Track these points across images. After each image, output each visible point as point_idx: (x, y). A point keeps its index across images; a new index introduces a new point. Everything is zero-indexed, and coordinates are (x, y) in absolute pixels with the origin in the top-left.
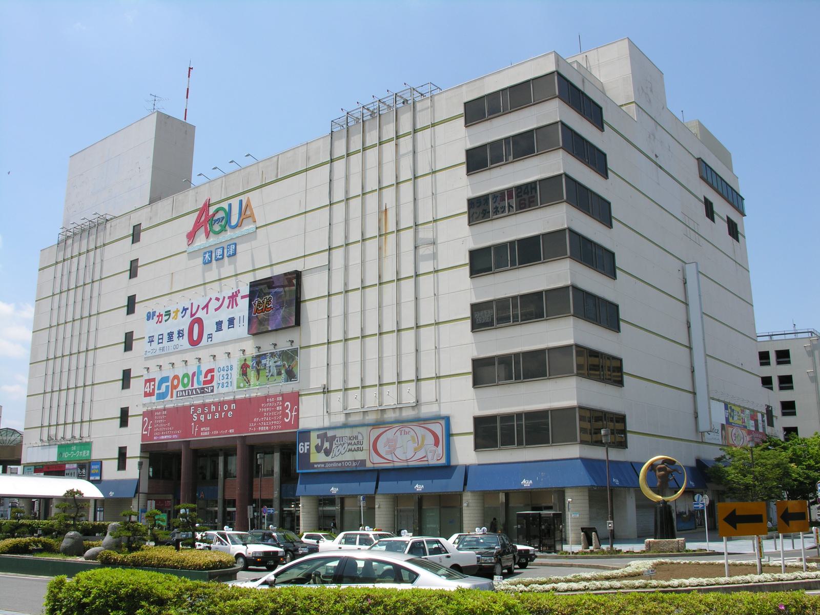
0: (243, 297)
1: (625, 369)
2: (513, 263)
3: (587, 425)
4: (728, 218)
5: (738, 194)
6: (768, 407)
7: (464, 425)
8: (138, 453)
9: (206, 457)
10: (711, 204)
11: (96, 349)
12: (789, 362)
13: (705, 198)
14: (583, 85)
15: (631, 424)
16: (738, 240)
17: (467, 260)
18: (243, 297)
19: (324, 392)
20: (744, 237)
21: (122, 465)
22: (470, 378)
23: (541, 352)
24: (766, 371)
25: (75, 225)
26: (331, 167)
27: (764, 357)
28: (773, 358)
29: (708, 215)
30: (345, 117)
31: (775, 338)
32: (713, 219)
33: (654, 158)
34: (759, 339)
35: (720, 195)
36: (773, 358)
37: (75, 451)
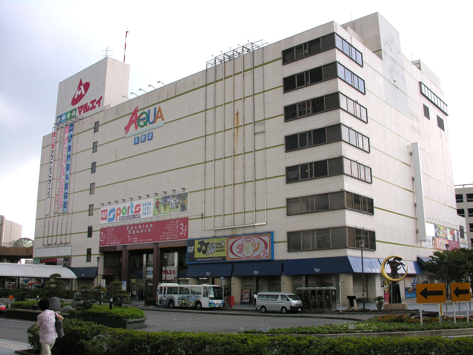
1: (375, 205)
7: (281, 236)
8: (98, 252)
24: (462, 206)
27: (459, 198)
28: (465, 198)
35: (433, 109)
36: (465, 198)
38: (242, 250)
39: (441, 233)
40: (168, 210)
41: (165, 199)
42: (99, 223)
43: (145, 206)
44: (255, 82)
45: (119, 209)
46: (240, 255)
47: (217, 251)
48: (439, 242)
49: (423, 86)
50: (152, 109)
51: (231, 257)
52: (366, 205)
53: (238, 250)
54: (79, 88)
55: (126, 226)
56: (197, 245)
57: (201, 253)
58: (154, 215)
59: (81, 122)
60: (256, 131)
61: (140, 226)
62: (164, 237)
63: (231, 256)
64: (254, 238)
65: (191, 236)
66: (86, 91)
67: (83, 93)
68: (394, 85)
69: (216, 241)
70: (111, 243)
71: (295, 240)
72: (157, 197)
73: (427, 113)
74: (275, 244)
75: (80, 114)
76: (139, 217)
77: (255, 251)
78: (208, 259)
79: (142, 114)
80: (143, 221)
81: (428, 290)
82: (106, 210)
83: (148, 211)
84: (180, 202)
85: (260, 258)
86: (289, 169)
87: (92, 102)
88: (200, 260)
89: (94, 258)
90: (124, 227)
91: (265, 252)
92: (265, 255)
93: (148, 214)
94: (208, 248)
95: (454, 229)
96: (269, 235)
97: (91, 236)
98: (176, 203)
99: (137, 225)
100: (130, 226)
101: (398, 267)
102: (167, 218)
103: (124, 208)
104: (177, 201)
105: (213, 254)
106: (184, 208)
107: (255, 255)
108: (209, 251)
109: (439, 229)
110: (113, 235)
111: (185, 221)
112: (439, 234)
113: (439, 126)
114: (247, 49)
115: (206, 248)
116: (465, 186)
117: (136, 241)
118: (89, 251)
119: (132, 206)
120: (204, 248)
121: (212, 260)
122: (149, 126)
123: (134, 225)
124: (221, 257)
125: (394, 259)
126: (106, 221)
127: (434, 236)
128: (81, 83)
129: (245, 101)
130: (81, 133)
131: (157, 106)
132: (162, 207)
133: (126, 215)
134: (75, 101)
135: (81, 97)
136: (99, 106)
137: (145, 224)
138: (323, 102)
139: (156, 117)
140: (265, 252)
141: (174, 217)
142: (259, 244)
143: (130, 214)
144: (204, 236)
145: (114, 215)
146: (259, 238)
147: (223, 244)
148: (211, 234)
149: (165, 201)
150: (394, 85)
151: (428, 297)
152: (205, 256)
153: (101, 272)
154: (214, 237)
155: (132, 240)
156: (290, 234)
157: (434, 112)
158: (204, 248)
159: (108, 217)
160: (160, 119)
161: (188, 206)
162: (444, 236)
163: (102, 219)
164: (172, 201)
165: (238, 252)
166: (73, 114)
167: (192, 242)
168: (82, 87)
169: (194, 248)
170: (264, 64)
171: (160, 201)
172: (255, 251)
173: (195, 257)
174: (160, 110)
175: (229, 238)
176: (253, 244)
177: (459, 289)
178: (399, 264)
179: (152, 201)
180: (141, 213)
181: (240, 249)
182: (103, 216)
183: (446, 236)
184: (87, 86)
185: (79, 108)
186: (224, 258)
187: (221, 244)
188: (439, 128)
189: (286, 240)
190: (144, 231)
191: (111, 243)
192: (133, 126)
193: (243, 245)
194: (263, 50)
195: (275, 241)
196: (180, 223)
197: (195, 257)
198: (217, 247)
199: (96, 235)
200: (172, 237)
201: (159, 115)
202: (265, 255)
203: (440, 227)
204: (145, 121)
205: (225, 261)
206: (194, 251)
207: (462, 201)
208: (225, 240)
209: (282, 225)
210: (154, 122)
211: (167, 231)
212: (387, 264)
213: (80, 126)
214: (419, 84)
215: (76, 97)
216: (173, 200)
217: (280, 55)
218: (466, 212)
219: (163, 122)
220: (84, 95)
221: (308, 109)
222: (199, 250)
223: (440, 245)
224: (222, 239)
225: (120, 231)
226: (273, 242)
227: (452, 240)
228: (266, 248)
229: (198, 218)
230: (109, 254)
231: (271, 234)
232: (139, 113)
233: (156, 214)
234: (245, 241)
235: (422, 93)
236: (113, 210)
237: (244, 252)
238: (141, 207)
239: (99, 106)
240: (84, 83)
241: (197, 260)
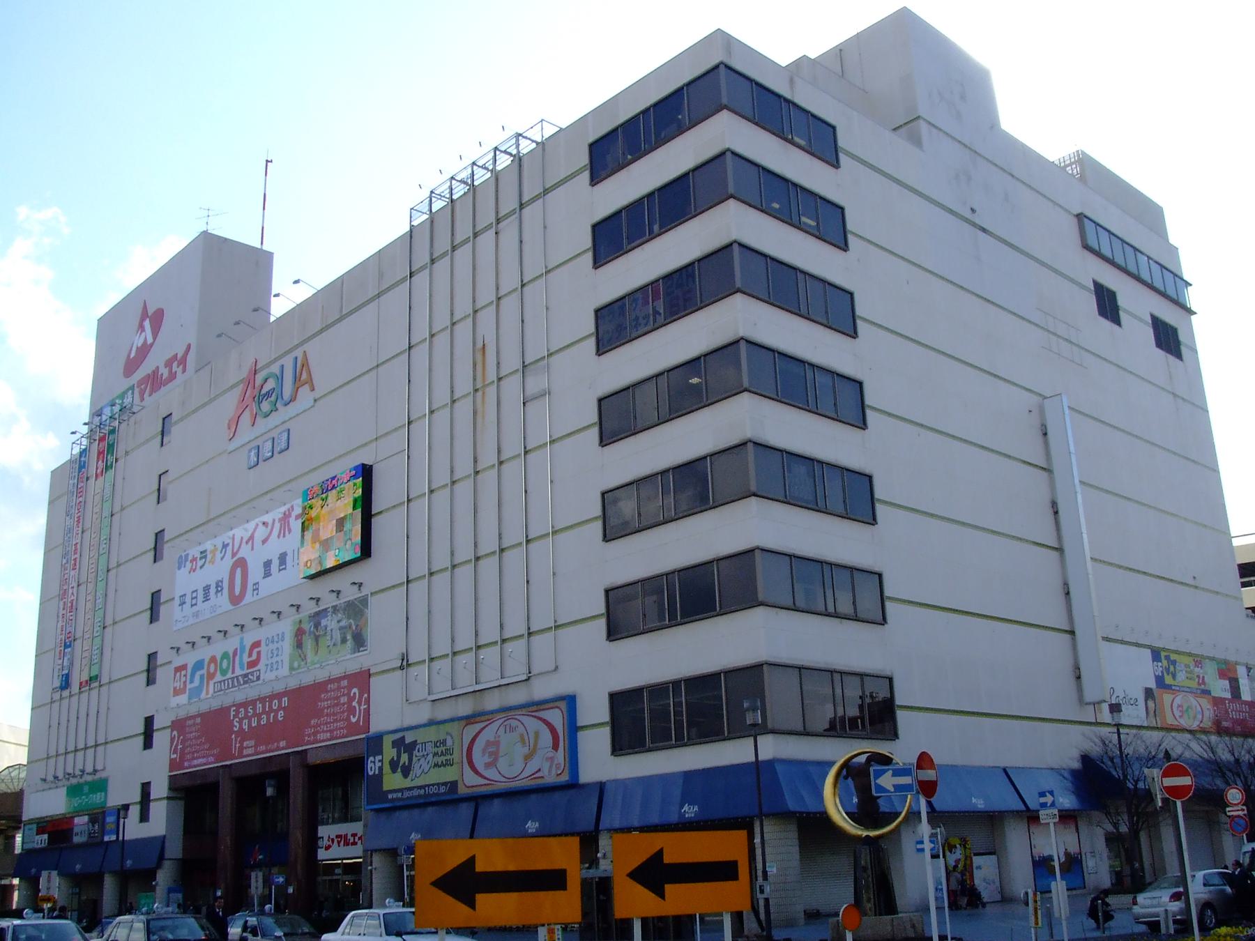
19: (401, 668)
32: (1116, 320)
33: (968, 214)
38: (496, 759)
39: (1181, 676)
40: (323, 650)
41: (317, 617)
42: (170, 703)
43: (271, 646)
44: (526, 247)
45: (213, 659)
46: (491, 773)
47: (436, 765)
48: (1175, 705)
49: (1089, 227)
50: (288, 362)
51: (470, 782)
53: (487, 759)
54: (141, 328)
55: (228, 709)
56: (389, 752)
57: (399, 775)
58: (292, 669)
60: (529, 392)
61: (259, 705)
62: (315, 734)
63: (470, 779)
64: (526, 720)
65: (376, 726)
66: (155, 334)
67: (150, 340)
68: (974, 225)
69: (432, 734)
70: (195, 762)
71: (639, 718)
72: (297, 617)
73: (1107, 305)
74: (580, 734)
75: (142, 400)
76: (258, 678)
77: (528, 758)
78: (416, 793)
79: (266, 380)
80: (266, 691)
81: (667, 859)
82: (184, 667)
83: (279, 659)
84: (350, 626)
85: (540, 781)
87: (169, 364)
88: (395, 796)
89: (159, 810)
90: (223, 712)
91: (552, 759)
92: (554, 772)
93: (280, 671)
94: (415, 759)
95: (1237, 663)
96: (563, 705)
98: (341, 628)
99: (253, 703)
100: (239, 706)
102: (321, 675)
103: (225, 655)
104: (343, 623)
105: (427, 775)
106: (359, 641)
107: (527, 773)
108: (416, 770)
109: (1174, 663)
110: (199, 737)
111: (362, 679)
112: (1174, 676)
113: (1159, 344)
115: (410, 760)
117: (250, 751)
118: (146, 787)
119: (243, 647)
120: (404, 758)
121: (425, 796)
122: (284, 413)
123: (244, 705)
124: (445, 784)
125: (869, 760)
126: (183, 699)
127: (1152, 684)
128: (145, 314)
129: (502, 307)
131: (299, 353)
132: (308, 643)
133: (229, 675)
134: (131, 366)
135: (144, 350)
136: (184, 371)
137: (272, 697)
138: (694, 282)
139: (297, 382)
140: (552, 759)
141: (337, 671)
142: (537, 734)
143: (239, 672)
144: (408, 722)
145: (202, 676)
146: (540, 719)
147: (449, 742)
148: (422, 714)
149: (317, 625)
150: (974, 225)
151: (669, 888)
152: (407, 783)
153: (175, 850)
154: (431, 723)
155: (242, 748)
156: (618, 700)
157: (1129, 295)
158: (404, 758)
159: (189, 686)
160: (307, 387)
161: (371, 634)
162: (1193, 684)
163: (177, 692)
164: (330, 623)
165: (488, 765)
166: (127, 401)
167: (375, 744)
168: (147, 324)
169: (381, 761)
170: (546, 191)
171: (307, 626)
172: (528, 758)
173: (385, 788)
174: (305, 364)
175: (463, 723)
176: (522, 736)
179: (286, 627)
180: (261, 666)
181: (491, 754)
182: (177, 685)
183: (1204, 683)
184: (157, 319)
185: (140, 383)
186: (453, 785)
187: (444, 742)
188: (1160, 353)
189: (607, 718)
190: (268, 719)
191: (195, 762)
192: (246, 418)
193: (497, 743)
194: (544, 150)
195: (579, 724)
196: (350, 688)
197: (385, 788)
198: (435, 754)
199: (162, 739)
200: (331, 731)
201: (304, 376)
202: (554, 772)
203: (1173, 657)
204: (273, 398)
205: (456, 796)
206: (381, 769)
208: (454, 728)
209: (603, 669)
210: (293, 399)
211: (318, 713)
212: (846, 778)
214: (1075, 220)
215: (133, 355)
216: (336, 618)
217: (584, 159)
219: (312, 396)
220: (152, 345)
221: (654, 308)
222: (394, 765)
223: (1177, 714)
224: (447, 727)
225: (214, 724)
226: (574, 729)
227: (1228, 696)
228: (555, 747)
229: (394, 669)
230: (193, 794)
231: (570, 701)
232: (259, 378)
233: (296, 665)
234: (502, 729)
235: (1086, 247)
236: (199, 665)
237: (502, 764)
238: (263, 648)
239: (184, 371)
240: (150, 312)
241: (390, 796)
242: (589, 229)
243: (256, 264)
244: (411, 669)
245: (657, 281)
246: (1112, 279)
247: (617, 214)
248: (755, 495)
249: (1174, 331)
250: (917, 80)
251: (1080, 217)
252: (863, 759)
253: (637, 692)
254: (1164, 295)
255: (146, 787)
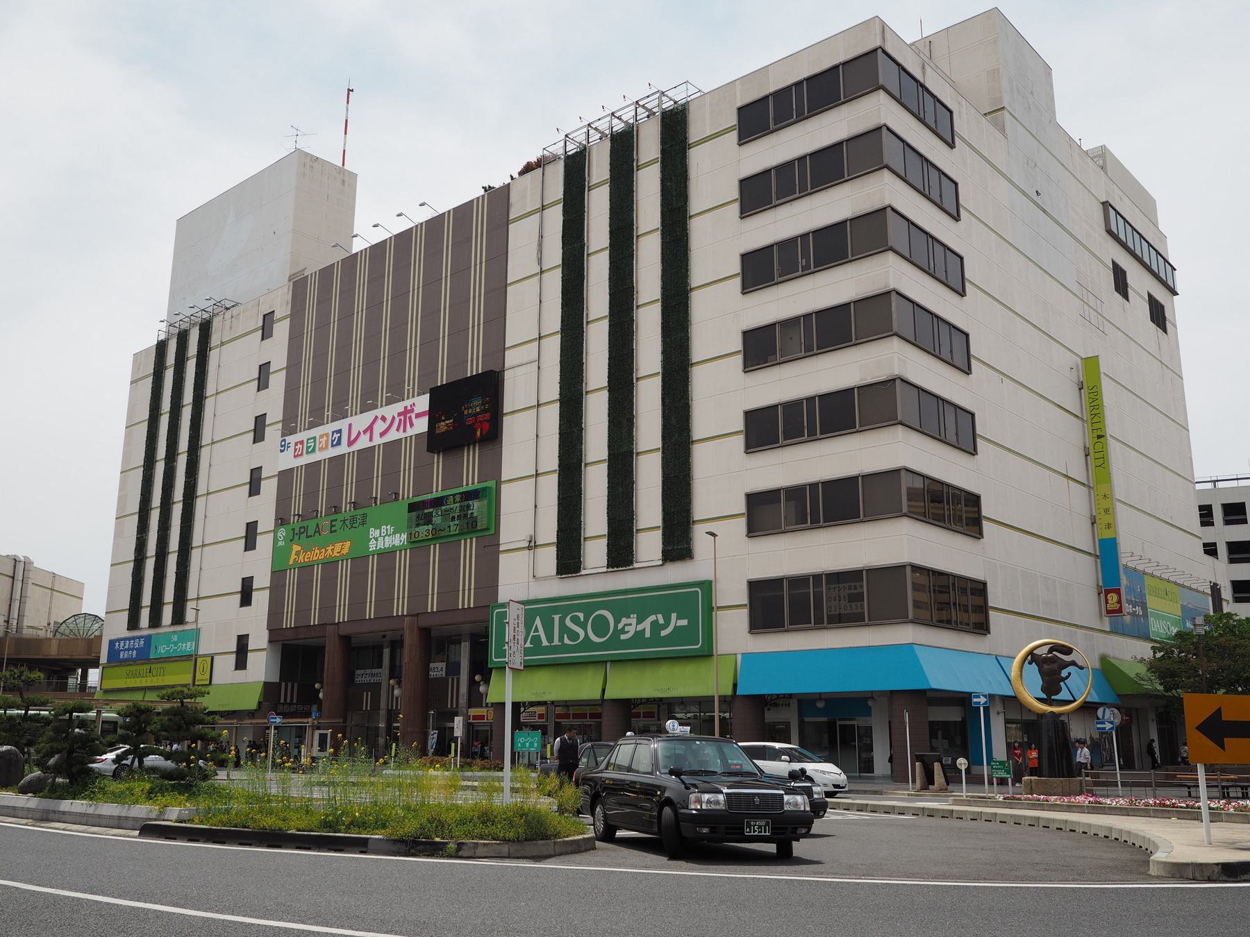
0: (418, 416)
1: (985, 511)
2: (812, 433)
3: (924, 597)
4: (1150, 295)
5: (1166, 261)
6: (1216, 584)
7: (732, 592)
8: (264, 642)
9: (361, 649)
10: (1124, 273)
11: (203, 546)
12: (1245, 521)
13: (1114, 263)
14: (924, 73)
15: (995, 597)
16: (1165, 331)
17: (740, 426)
18: (418, 416)
19: (529, 548)
20: (1175, 326)
21: (241, 664)
22: (742, 523)
23: (851, 482)
24: (1209, 534)
25: (181, 317)
26: (542, 218)
27: (1206, 515)
28: (1218, 515)
29: (1117, 289)
30: (562, 144)
31: (1220, 485)
32: (1126, 296)
33: (1034, 196)
34: (1199, 487)
35: (1137, 265)
36: (1218, 515)
37: (175, 644)
49: (1112, 213)
52: (957, 510)
59: (229, 313)
86: (751, 417)
97: (249, 604)
101: (1064, 673)
114: (648, 110)
116: (1220, 485)
118: (242, 641)
125: (1050, 651)
130: (228, 342)
156: (756, 587)
157: (1138, 280)
177: (1225, 717)
178: (1067, 665)
189: (745, 601)
207: (1212, 524)
212: (1030, 663)
213: (228, 323)
218: (1222, 550)
235: (1109, 232)
242: (736, 184)
243: (344, 181)
244: (538, 550)
245: (807, 234)
246: (1126, 262)
247: (766, 172)
248: (902, 424)
249: (1162, 307)
250: (1019, 83)
251: (1106, 205)
252: (1045, 650)
253: (776, 583)
254: (1156, 276)
255: (242, 641)
